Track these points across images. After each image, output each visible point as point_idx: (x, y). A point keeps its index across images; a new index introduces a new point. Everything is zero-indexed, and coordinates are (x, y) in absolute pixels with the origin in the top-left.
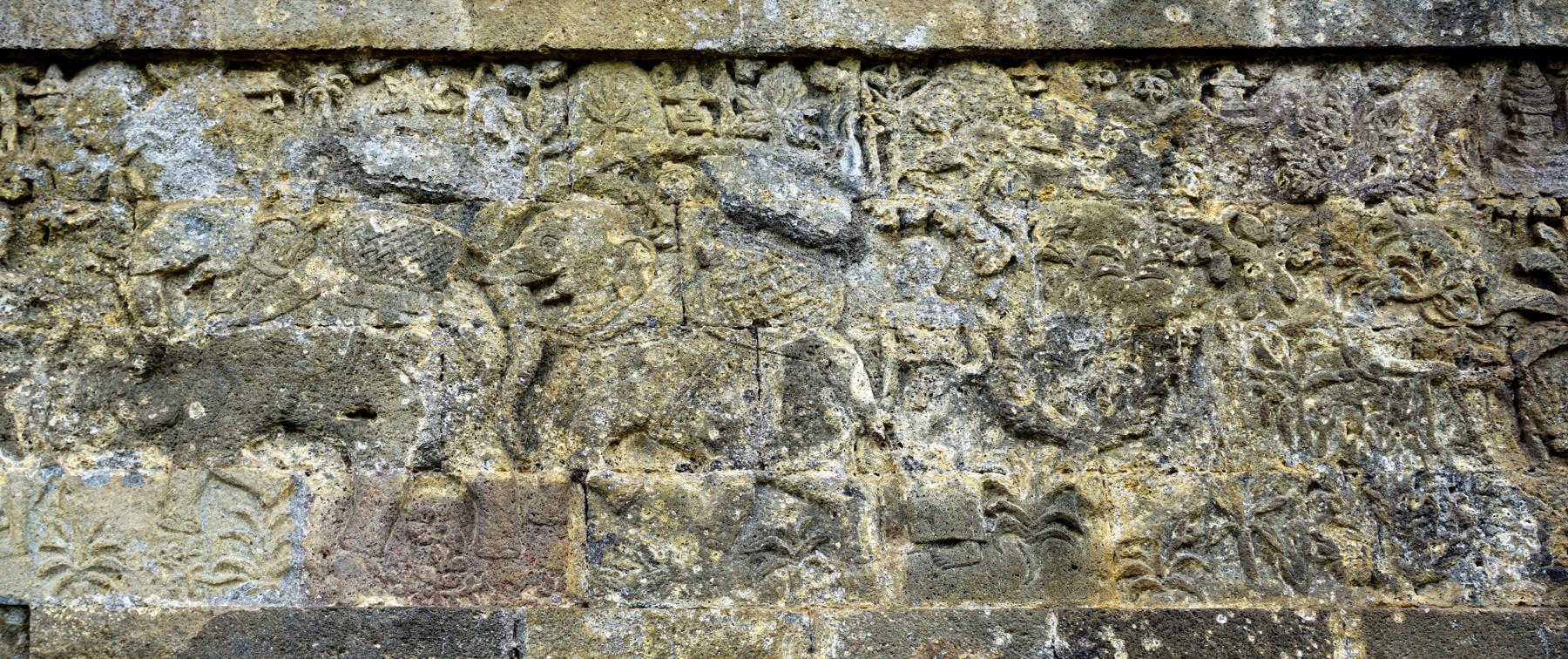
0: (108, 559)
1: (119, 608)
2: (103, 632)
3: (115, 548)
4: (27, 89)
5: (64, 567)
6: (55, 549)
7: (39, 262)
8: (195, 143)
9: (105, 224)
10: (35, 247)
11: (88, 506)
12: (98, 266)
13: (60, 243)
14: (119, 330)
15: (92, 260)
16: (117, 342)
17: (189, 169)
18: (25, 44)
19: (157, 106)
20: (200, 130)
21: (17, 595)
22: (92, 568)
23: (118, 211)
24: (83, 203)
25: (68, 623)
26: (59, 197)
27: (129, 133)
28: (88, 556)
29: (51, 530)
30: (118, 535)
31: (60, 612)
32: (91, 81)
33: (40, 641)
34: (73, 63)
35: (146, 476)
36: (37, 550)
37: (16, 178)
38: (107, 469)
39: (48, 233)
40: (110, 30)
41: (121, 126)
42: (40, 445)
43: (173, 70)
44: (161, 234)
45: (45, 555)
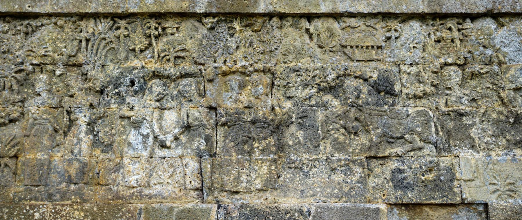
0: (512, 187)
1: (517, 204)
2: (516, 212)
3: (513, 184)
4: (460, 27)
5: (498, 190)
6: (494, 184)
7: (470, 86)
8: (517, 45)
9: (492, 73)
10: (469, 81)
11: (502, 169)
12: (491, 87)
13: (477, 79)
14: (500, 109)
15: (489, 85)
16: (500, 113)
17: (515, 53)
18: (463, 11)
19: (503, 32)
20: (518, 40)
21: (484, 200)
22: (507, 190)
23: (496, 68)
24: (484, 65)
25: (502, 210)
26: (477, 64)
27: (496, 41)
28: (505, 186)
29: (492, 177)
30: (514, 179)
31: (498, 206)
32: (481, 24)
33: (494, 216)
34: (474, 17)
35: (518, 159)
36: (488, 184)
37: (462, 57)
38: (505, 156)
39: (473, 76)
40: (490, 6)
41: (493, 39)
42: (484, 149)
43: (507, 20)
44: (512, 76)
45: (491, 186)
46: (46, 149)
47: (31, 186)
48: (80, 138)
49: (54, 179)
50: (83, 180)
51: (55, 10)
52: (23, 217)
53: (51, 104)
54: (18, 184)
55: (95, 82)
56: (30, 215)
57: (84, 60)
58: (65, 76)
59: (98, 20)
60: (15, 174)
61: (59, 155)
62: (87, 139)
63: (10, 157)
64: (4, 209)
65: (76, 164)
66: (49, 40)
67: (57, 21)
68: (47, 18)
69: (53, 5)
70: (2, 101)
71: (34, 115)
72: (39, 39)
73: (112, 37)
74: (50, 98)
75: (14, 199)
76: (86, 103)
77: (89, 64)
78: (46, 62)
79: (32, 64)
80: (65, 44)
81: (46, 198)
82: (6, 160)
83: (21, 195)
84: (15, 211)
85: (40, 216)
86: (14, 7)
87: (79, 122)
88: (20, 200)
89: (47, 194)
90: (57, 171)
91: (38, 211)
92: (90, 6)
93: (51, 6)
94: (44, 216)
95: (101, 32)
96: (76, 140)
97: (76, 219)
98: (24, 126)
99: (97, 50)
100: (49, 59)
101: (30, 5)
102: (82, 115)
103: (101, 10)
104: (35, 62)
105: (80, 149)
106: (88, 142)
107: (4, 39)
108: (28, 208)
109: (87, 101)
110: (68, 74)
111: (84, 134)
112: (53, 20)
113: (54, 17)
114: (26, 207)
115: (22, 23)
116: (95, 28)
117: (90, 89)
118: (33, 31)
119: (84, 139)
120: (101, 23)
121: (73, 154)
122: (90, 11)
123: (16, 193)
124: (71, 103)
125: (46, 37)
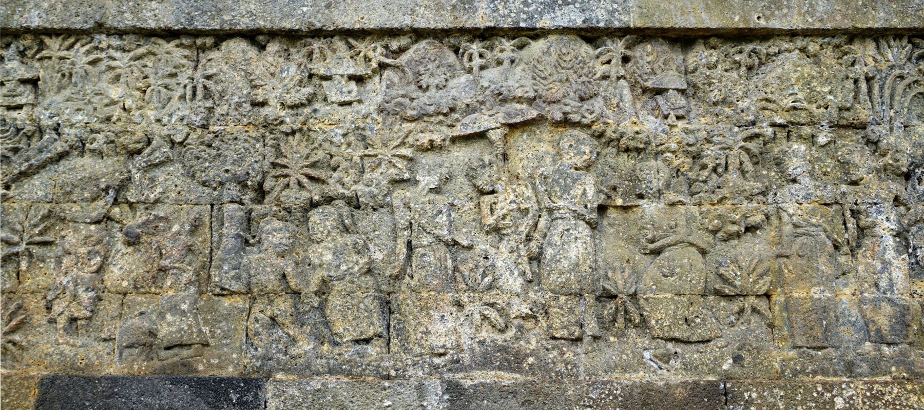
46: (826, 280)
47: (808, 348)
48: (887, 260)
49: (847, 336)
50: (908, 337)
51: (810, 24)
52: (814, 405)
53: (822, 197)
54: (781, 346)
55: (898, 156)
56: (825, 403)
57: (870, 115)
58: (832, 146)
59: (883, 43)
60: (771, 326)
61: (848, 291)
62: (902, 262)
63: (758, 296)
64: (775, 391)
65: (887, 309)
66: (798, 80)
67: (808, 44)
68: (787, 39)
69: (804, 14)
70: (730, 193)
71: (794, 218)
72: (779, 78)
73: (914, 74)
74: (819, 186)
75: (783, 372)
76: (888, 195)
77: (879, 124)
78: (798, 120)
79: (773, 125)
80: (830, 88)
81: (842, 372)
82: (752, 300)
83: (795, 365)
84: (796, 395)
85: (846, 403)
86: (732, 19)
87: (879, 230)
88: (795, 375)
89: (842, 363)
90: (849, 321)
91: (841, 395)
92: (874, 16)
93: (802, 17)
94: (854, 404)
95: (894, 63)
96: (880, 264)
97: (915, 409)
98: (772, 239)
99: (892, 96)
100: (803, 114)
101: (761, 15)
102: (883, 217)
103: (896, 22)
104: (779, 120)
105: (891, 280)
106: (903, 268)
107: (714, 79)
108: (820, 389)
109: (890, 192)
110: (839, 142)
111: (892, 251)
112: (800, 43)
113: (800, 38)
114: (815, 387)
115: (741, 49)
116: (879, 57)
117: (885, 170)
118: (761, 64)
119: (896, 262)
120: (889, 47)
121: (878, 290)
122: (876, 26)
123: (784, 361)
124: (859, 196)
125: (792, 75)
